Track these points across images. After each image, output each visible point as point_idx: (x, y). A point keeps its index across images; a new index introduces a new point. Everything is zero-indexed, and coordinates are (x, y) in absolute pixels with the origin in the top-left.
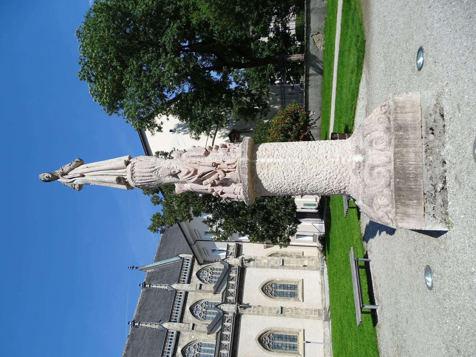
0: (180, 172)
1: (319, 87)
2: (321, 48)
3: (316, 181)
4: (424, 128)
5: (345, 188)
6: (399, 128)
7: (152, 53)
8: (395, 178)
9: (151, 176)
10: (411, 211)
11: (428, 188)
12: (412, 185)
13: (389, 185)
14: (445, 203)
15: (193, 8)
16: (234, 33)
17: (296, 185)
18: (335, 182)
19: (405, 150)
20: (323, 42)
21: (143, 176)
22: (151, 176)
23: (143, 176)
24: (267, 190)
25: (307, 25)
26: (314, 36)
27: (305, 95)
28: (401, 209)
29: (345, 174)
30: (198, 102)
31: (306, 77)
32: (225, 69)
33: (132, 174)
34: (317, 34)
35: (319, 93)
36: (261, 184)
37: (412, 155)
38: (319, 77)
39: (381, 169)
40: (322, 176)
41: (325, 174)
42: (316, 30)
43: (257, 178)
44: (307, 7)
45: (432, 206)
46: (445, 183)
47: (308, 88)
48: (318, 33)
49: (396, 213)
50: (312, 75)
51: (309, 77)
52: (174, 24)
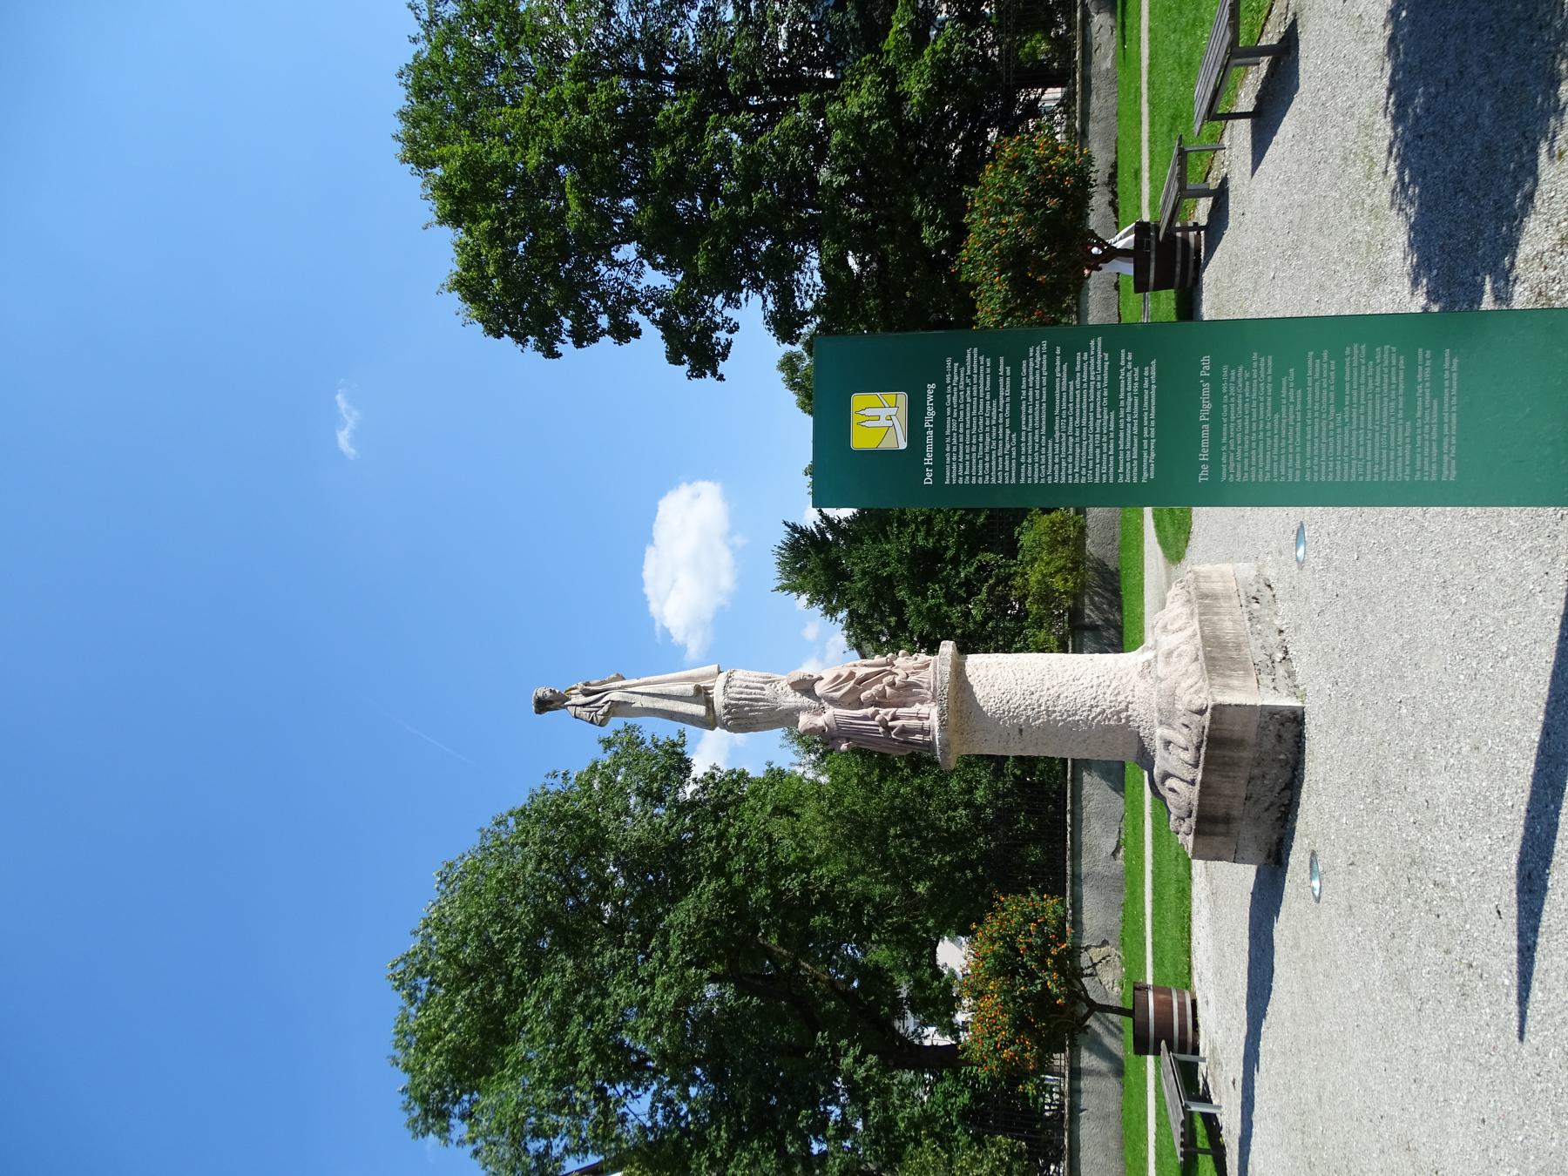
0: (821, 679)
1: (1113, 1120)
2: (1116, 989)
3: (1074, 689)
4: (1243, 596)
5: (1127, 709)
6: (1204, 596)
7: (627, 947)
8: (1204, 646)
9: (762, 689)
10: (1235, 683)
11: (1261, 657)
12: (1234, 654)
13: (1196, 659)
14: (1291, 674)
15: (769, 861)
16: (902, 770)
17: (1035, 697)
18: (1109, 692)
19: (1216, 618)
20: (1118, 972)
21: (747, 687)
22: (762, 689)
23: (747, 687)
24: (981, 708)
25: (1072, 915)
26: (1092, 949)
27: (1070, 1142)
28: (1218, 680)
29: (1124, 681)
30: (719, 1129)
31: (1071, 1078)
32: (823, 1038)
33: (728, 682)
34: (1100, 946)
35: (1113, 1145)
36: (972, 694)
37: (1229, 624)
38: (1111, 1084)
39: (1183, 647)
40: (1086, 682)
41: (1089, 679)
42: (1096, 933)
43: (966, 682)
44: (1073, 866)
45: (1271, 677)
46: (1286, 652)
47: (1078, 1119)
48: (1105, 943)
49: (1211, 686)
50: (1091, 1072)
51: (1079, 1079)
52: (709, 883)
